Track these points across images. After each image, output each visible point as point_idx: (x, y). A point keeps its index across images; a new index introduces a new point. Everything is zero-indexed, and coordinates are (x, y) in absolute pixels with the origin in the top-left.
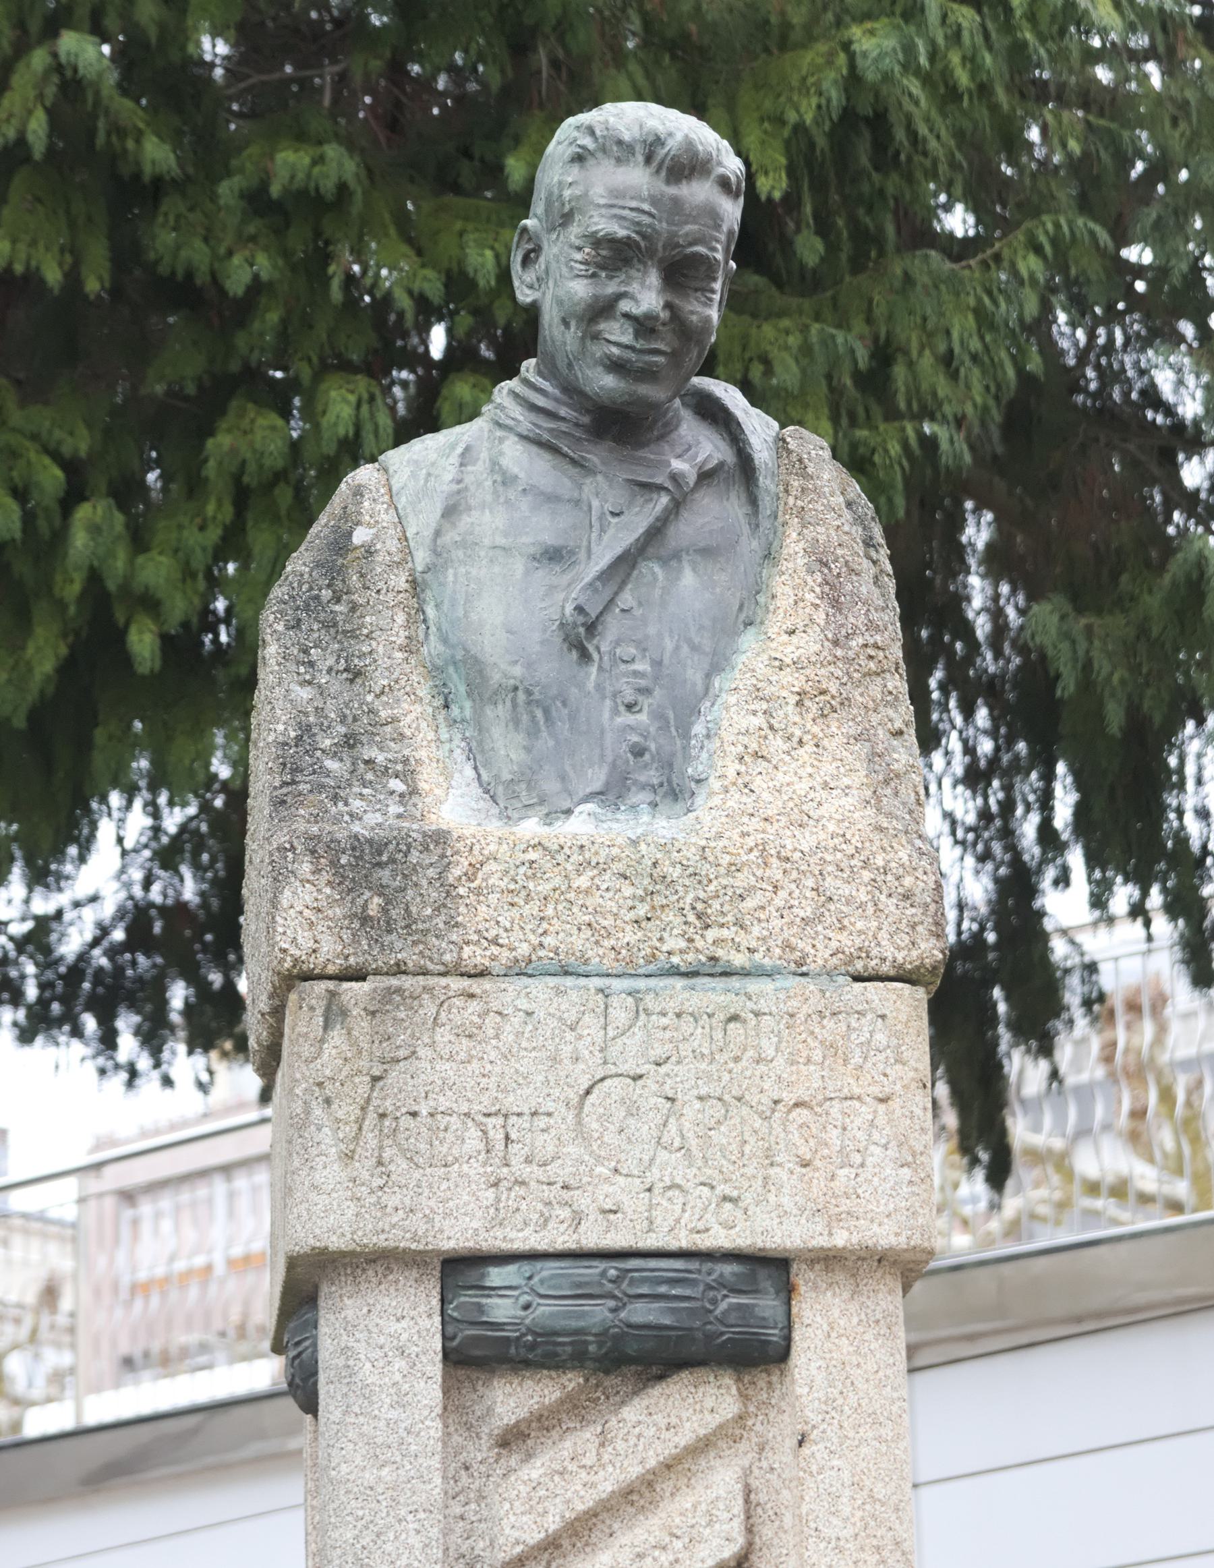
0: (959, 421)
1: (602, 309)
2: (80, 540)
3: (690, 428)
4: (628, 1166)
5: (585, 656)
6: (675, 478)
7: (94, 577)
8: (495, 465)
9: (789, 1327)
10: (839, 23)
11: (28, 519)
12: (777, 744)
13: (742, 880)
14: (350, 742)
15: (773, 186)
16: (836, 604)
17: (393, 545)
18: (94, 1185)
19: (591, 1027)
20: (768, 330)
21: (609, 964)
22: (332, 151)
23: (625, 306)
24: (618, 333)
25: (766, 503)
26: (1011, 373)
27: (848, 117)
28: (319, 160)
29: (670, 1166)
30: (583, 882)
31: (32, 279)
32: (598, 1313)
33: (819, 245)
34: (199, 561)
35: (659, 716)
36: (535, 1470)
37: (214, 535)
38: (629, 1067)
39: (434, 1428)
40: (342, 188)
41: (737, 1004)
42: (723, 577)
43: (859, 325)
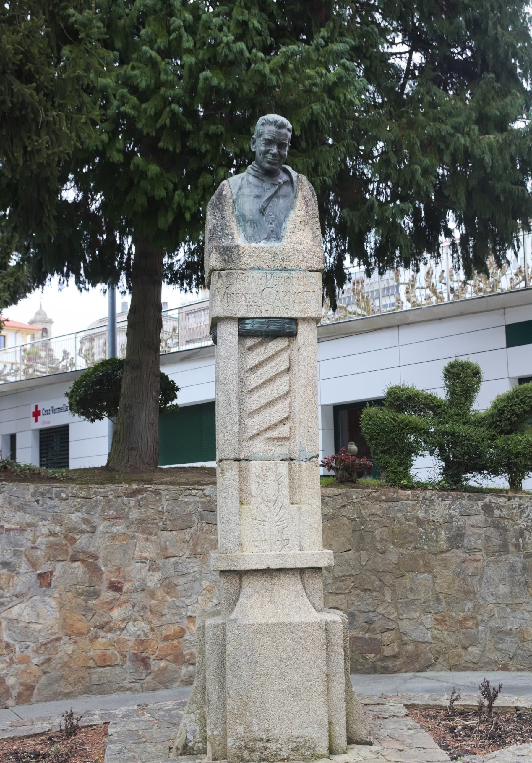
0: (330, 177)
1: (266, 152)
2: (176, 197)
3: (282, 174)
4: (270, 303)
5: (263, 215)
6: (279, 183)
7: (179, 204)
8: (248, 180)
9: (297, 330)
10: (310, 103)
11: (167, 193)
12: (296, 230)
13: (290, 254)
14: (222, 229)
15: (297, 133)
16: (307, 206)
17: (230, 195)
18: (181, 311)
19: (264, 279)
20: (297, 159)
21: (267, 268)
22: (220, 126)
23: (271, 152)
24: (269, 157)
25: (295, 188)
26: (339, 168)
27: (311, 120)
28: (218, 128)
29: (277, 303)
30: (262, 254)
31: (167, 149)
32: (265, 328)
33: (305, 144)
34: (197, 201)
35: (276, 225)
36: (254, 354)
37: (200, 196)
38: (270, 286)
39: (237, 347)
40: (222, 133)
41: (289, 275)
42: (287, 201)
43: (313, 159)
